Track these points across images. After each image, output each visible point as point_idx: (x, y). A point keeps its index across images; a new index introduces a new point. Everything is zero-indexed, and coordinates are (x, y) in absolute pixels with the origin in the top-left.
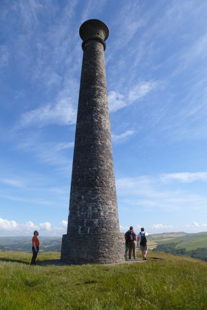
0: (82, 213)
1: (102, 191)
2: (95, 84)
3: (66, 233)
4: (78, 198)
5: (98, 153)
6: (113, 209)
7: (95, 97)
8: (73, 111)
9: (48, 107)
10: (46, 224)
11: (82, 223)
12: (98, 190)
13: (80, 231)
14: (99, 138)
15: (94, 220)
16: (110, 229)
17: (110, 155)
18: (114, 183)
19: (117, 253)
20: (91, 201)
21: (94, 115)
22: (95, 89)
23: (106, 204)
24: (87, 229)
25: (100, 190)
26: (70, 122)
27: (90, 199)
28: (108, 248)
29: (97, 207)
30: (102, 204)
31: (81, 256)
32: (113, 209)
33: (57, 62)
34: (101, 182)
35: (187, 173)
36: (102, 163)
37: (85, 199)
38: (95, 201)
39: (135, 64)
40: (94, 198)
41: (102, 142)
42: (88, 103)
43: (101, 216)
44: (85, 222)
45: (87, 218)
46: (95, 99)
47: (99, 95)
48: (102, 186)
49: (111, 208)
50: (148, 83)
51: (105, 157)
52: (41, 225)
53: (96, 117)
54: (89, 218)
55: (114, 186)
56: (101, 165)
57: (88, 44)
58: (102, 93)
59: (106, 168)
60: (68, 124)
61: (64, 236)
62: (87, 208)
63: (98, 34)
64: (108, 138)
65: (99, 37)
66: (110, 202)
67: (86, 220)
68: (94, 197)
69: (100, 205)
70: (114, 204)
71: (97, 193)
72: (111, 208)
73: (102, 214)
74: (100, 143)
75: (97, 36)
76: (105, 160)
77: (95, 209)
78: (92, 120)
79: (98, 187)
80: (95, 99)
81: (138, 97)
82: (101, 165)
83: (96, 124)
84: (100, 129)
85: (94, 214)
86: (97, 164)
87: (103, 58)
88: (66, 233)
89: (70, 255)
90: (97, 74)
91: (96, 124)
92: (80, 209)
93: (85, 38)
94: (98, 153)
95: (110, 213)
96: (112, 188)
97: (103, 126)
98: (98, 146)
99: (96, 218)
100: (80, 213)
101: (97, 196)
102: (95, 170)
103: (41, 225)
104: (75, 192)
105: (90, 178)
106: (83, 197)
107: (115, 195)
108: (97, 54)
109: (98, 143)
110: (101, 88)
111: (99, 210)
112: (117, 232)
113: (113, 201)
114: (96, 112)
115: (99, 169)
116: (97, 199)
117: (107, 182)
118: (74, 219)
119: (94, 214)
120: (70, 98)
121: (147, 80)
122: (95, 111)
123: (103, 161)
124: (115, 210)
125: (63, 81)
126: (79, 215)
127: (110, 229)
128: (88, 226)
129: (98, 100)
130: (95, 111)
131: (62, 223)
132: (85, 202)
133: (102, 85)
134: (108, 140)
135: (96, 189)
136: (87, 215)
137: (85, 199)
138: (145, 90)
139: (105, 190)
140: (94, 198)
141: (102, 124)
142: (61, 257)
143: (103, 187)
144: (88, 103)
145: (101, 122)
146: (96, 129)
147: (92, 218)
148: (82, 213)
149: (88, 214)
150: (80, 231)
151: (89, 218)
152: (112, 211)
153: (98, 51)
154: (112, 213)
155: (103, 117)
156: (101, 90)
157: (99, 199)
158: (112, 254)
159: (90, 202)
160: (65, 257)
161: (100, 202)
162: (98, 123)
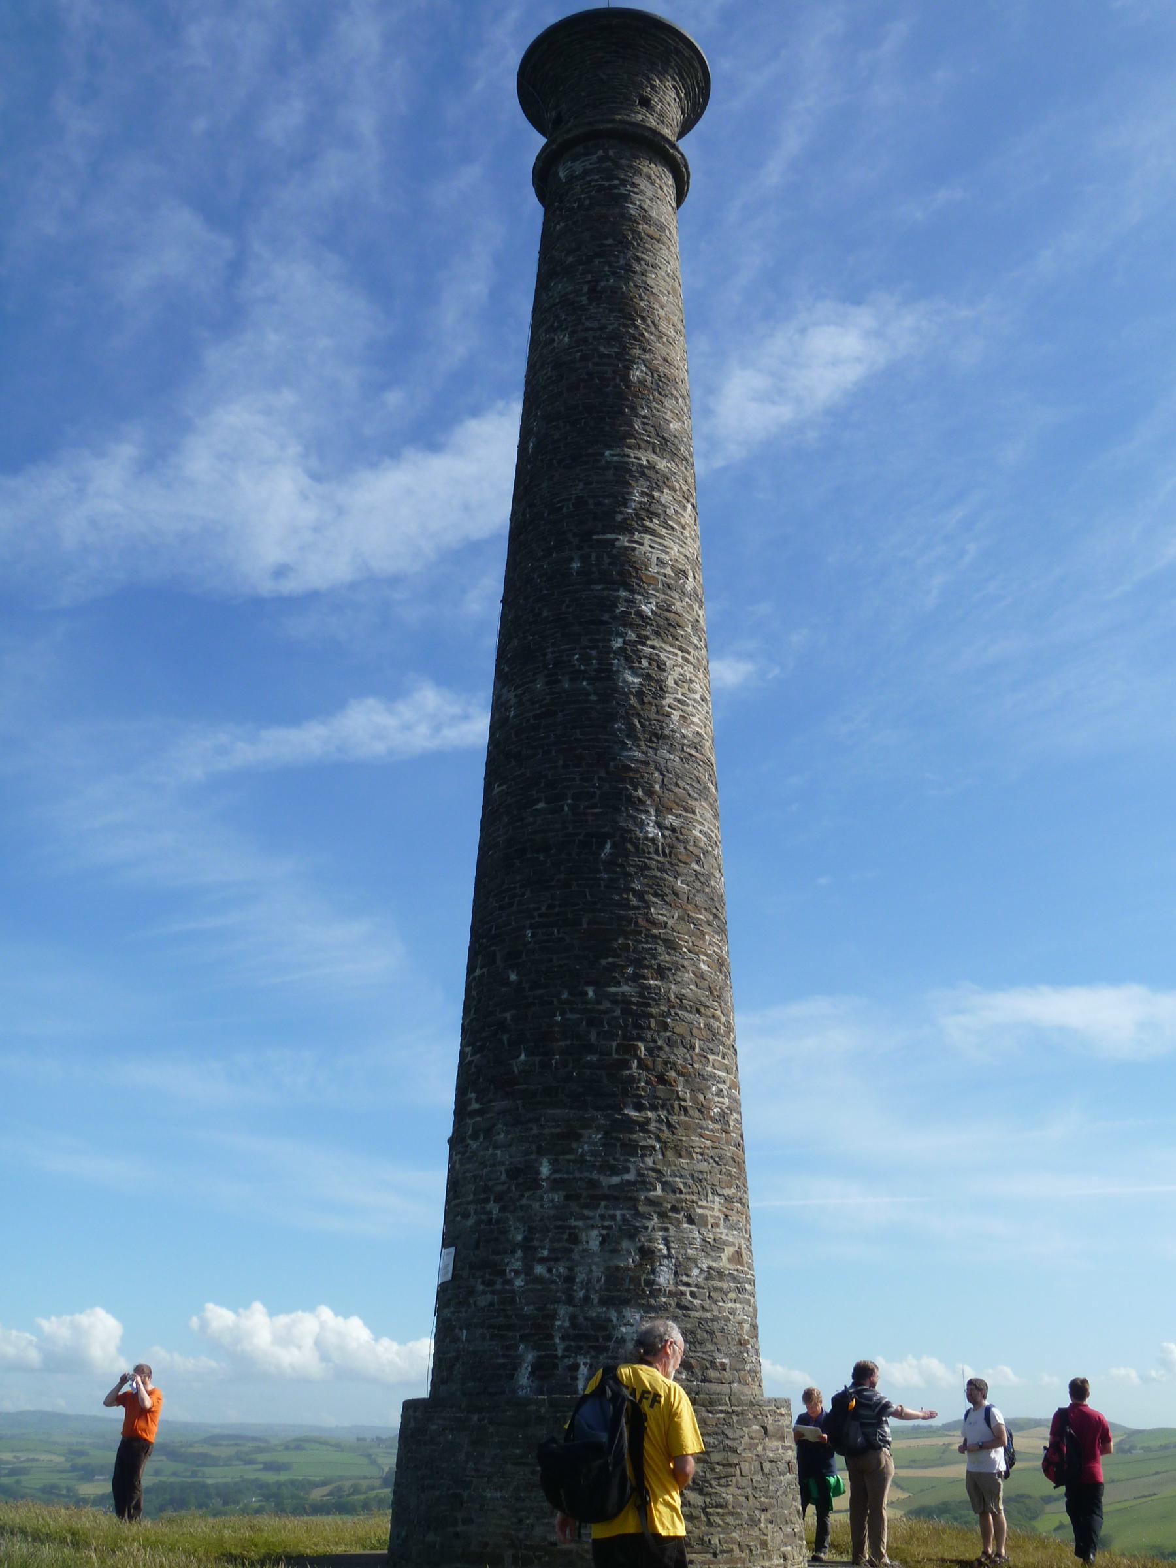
0: (539, 1270)
1: (666, 1134)
2: (621, 436)
3: (424, 1393)
4: (513, 1173)
5: (640, 895)
6: (729, 1251)
7: (625, 528)
8: (304, 497)
9: (127, 451)
10: (83, 1319)
11: (539, 1332)
12: (643, 1126)
13: (523, 1378)
14: (650, 793)
15: (613, 1315)
16: (712, 1373)
17: (715, 905)
18: (734, 1085)
19: (755, 1522)
20: (595, 1196)
21: (618, 644)
22: (624, 474)
23: (691, 1221)
24: (575, 1367)
25: (652, 1126)
26: (281, 572)
27: (593, 1184)
28: (701, 1492)
29: (632, 1234)
30: (663, 1215)
31: (539, 1531)
32: (729, 1251)
33: (200, 125)
34: (662, 1079)
35: (1135, 991)
36: (664, 957)
37: (556, 1185)
38: (626, 1196)
39: (773, 174)
40: (615, 1180)
41: (671, 819)
42: (576, 565)
43: (656, 1293)
44: (562, 1322)
45: (570, 1301)
46: (624, 541)
47: (653, 514)
48: (667, 1103)
49: (715, 1247)
50: (865, 317)
51: (686, 918)
52: (50, 1325)
53: (630, 657)
54: (587, 1299)
55: (736, 1104)
56: (661, 973)
57: (578, 167)
58: (666, 497)
59: (690, 991)
60: (267, 587)
61: (410, 1407)
62: (574, 1239)
63: (646, 103)
64: (704, 793)
65: (652, 122)
66: (712, 1207)
67: (563, 1311)
68: (614, 1171)
69: (655, 1221)
70: (734, 1218)
71: (632, 1149)
72: (715, 1247)
73: (664, 1278)
74: (652, 831)
75: (640, 116)
76: (685, 942)
77: (625, 1244)
78: (607, 675)
79: (639, 1107)
80: (624, 541)
81: (784, 412)
82: (661, 973)
83: (633, 700)
84: (658, 737)
85: (614, 1276)
86: (639, 963)
87: (673, 266)
88: (424, 1393)
89: (468, 1521)
90: (636, 374)
91: (633, 700)
92: (528, 1247)
93: (558, 121)
94: (640, 895)
95: (710, 1273)
96: (723, 1117)
97: (676, 716)
98: (642, 846)
99: (626, 1302)
100: (528, 1270)
101: (634, 1163)
102: (625, 1001)
103: (55, 1327)
104: (489, 1132)
105: (590, 1049)
106: (545, 1170)
107: (739, 1163)
108: (638, 236)
109: (642, 825)
110: (662, 465)
111: (647, 1254)
112: (747, 1392)
113: (728, 1199)
114: (631, 626)
115: (647, 997)
116: (634, 1183)
117: (698, 1082)
118: (483, 1301)
119: (614, 1276)
120: (288, 397)
121: (855, 296)
122: (625, 620)
123: (671, 946)
124: (738, 1257)
125: (236, 268)
126: (519, 1283)
127: (712, 1373)
128: (578, 1350)
129: (646, 547)
130: (625, 620)
131: (204, 1324)
132: (557, 1197)
133: (665, 445)
134: (702, 809)
135: (630, 1125)
136: (570, 1279)
137: (556, 1185)
138: (835, 362)
139: (687, 1127)
140: (615, 1180)
141: (669, 700)
142: (808, 1504)
143: (671, 1111)
144: (576, 565)
145: (661, 690)
146: (631, 732)
147: (603, 1302)
148: (539, 1270)
149: (581, 1277)
150: (523, 1378)
151: (587, 1299)
152: (724, 1262)
153: (647, 219)
154: (721, 1275)
155: (670, 656)
156: (663, 481)
157: (643, 1183)
158: (726, 1527)
159: (594, 1201)
160: (431, 1537)
161: (650, 1202)
162: (640, 694)
